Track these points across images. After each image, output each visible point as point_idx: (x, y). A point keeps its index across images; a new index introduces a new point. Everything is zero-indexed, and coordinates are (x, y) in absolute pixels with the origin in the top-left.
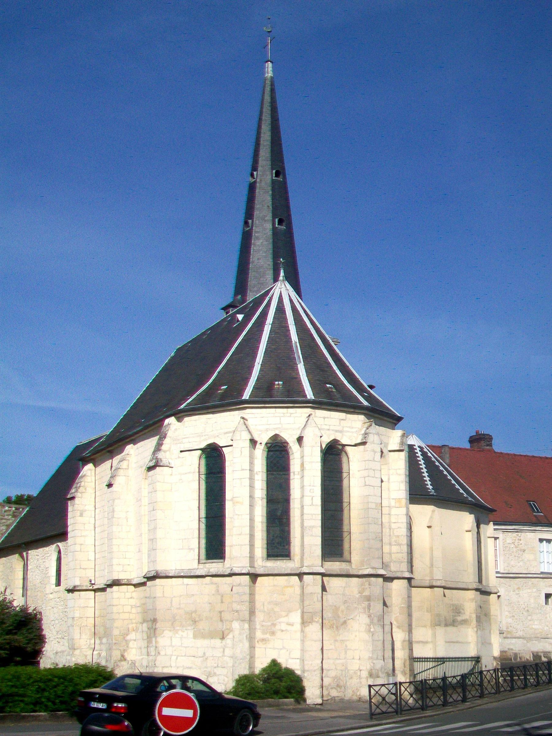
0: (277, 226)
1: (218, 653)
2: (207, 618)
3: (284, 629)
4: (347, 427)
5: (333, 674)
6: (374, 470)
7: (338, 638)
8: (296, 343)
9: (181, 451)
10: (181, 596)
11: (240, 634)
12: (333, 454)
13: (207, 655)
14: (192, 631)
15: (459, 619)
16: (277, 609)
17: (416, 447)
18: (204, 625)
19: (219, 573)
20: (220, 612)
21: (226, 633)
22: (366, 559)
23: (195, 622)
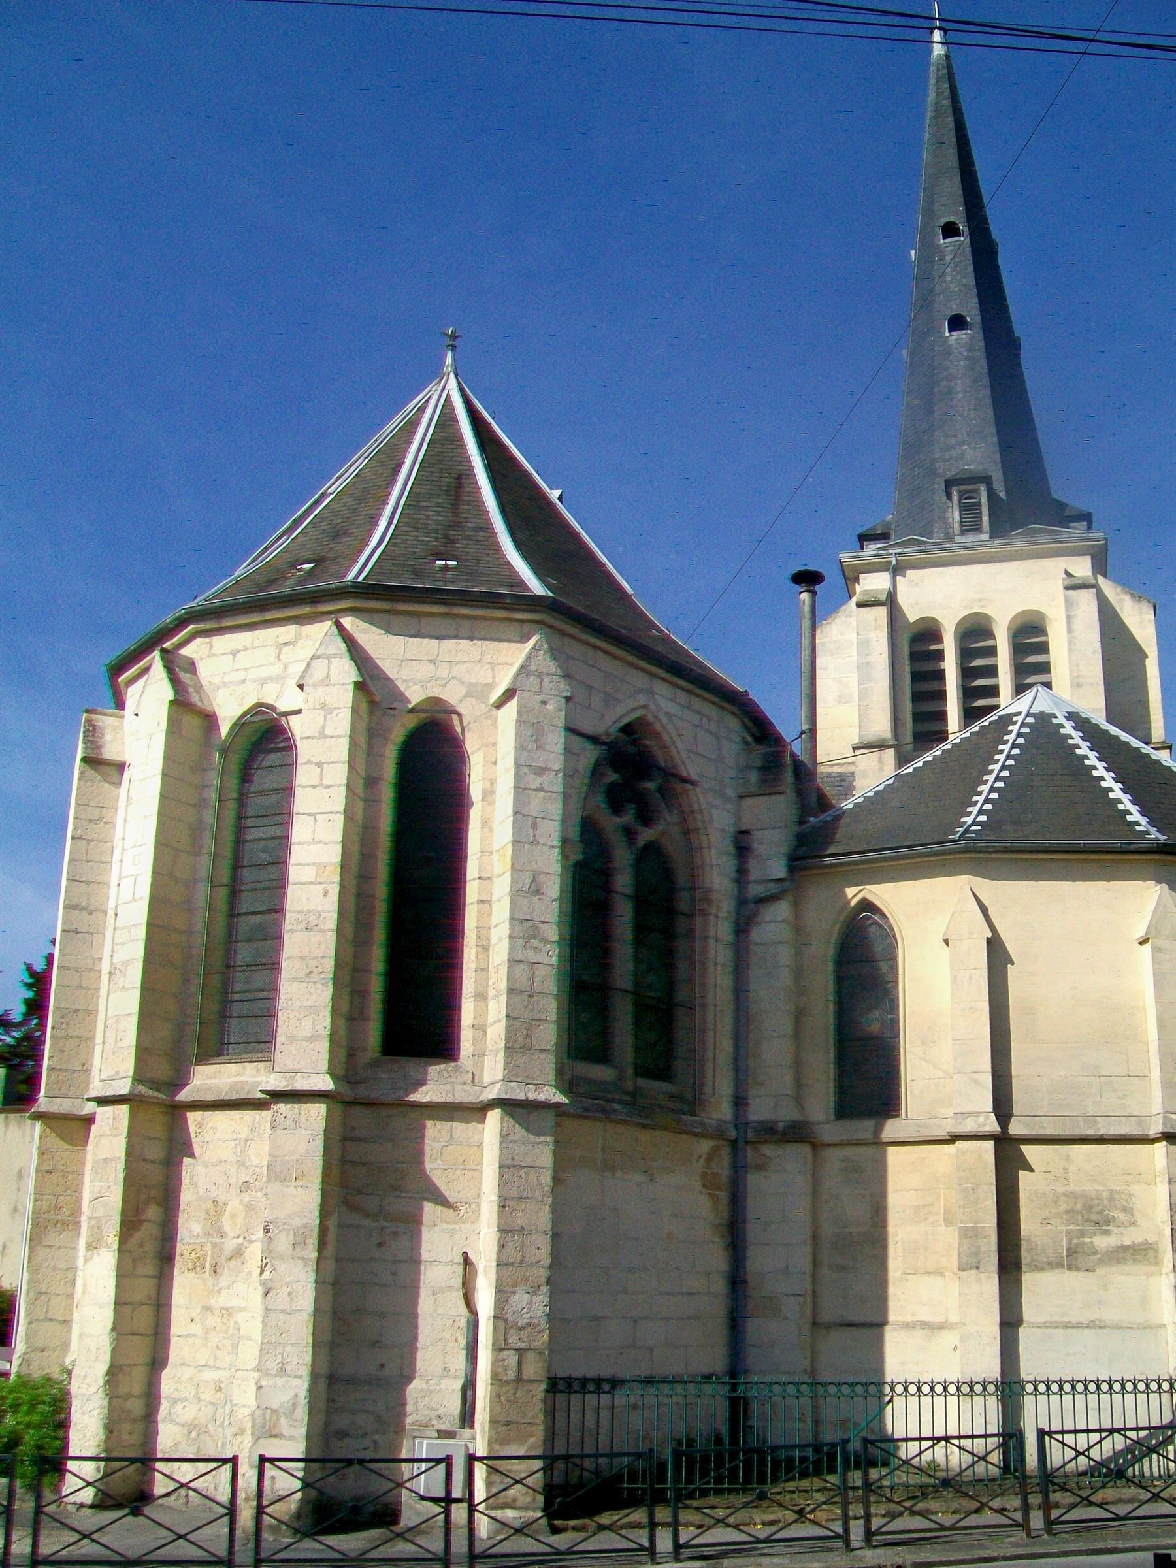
0: (947, 334)
5: (186, 1413)
6: (320, 765)
7: (213, 1302)
8: (324, 495)
15: (1102, 1242)
17: (1060, 719)
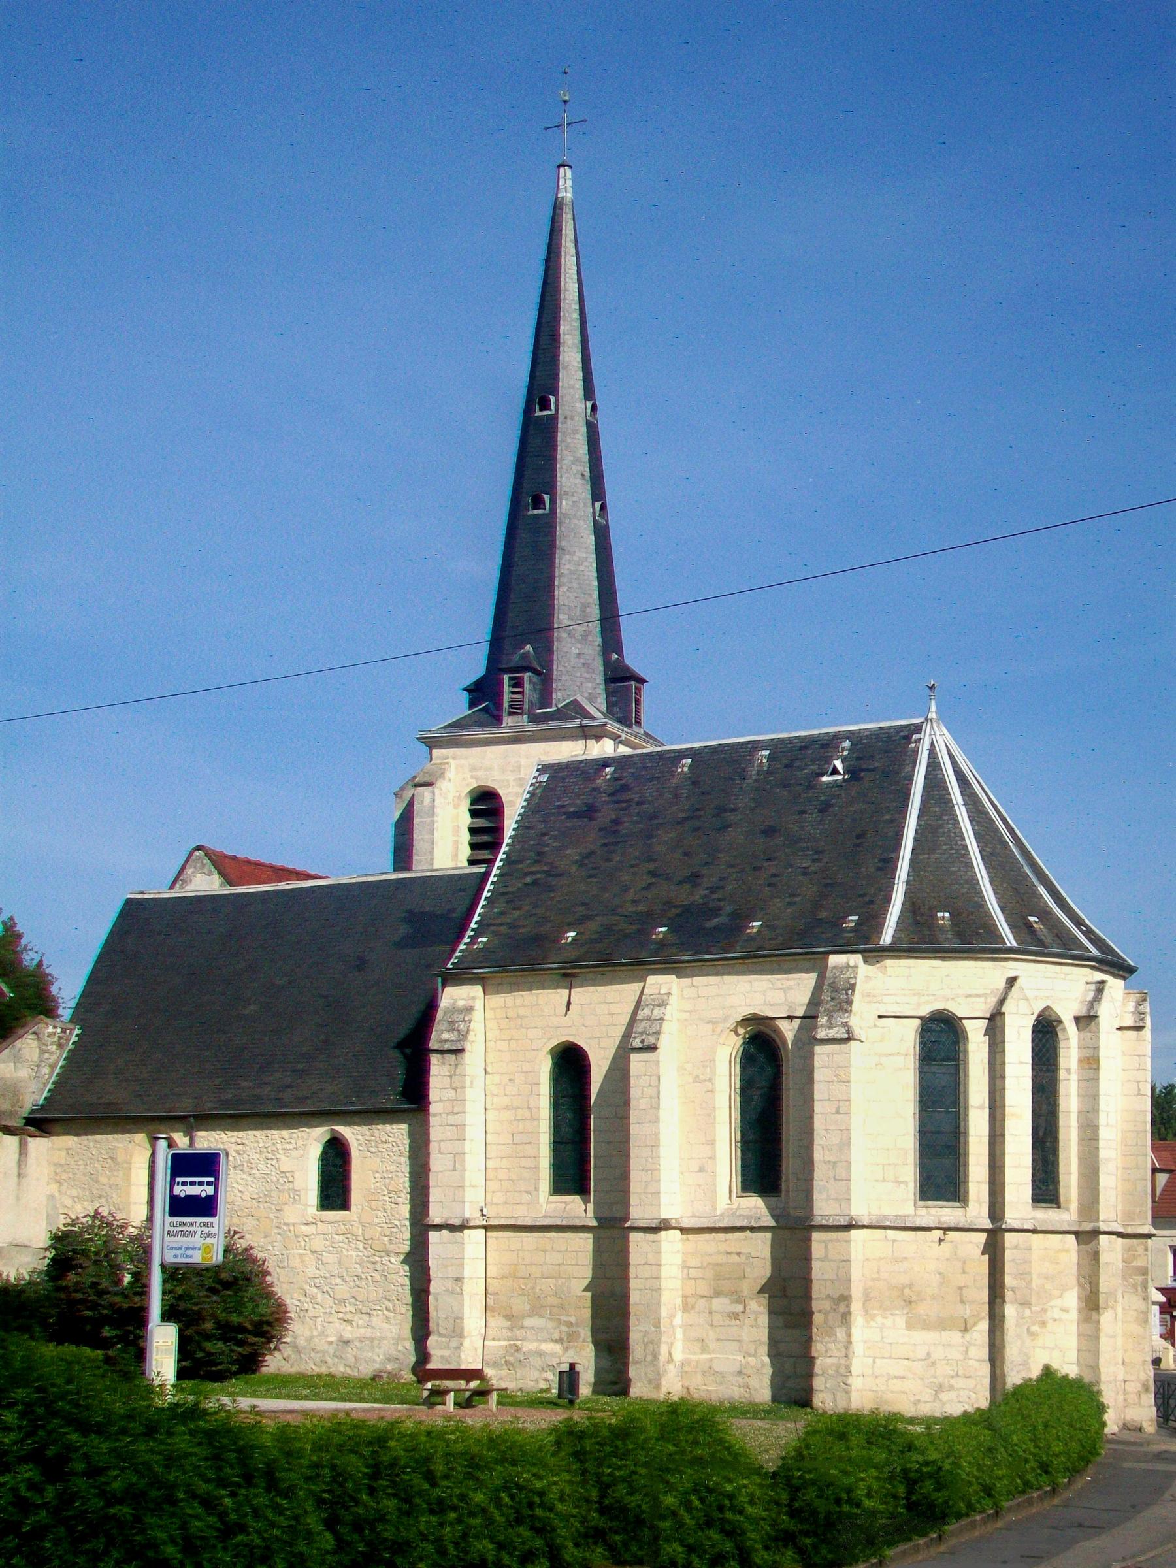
1: (955, 1354)
2: (933, 1298)
3: (1056, 1317)
4: (1058, 986)
9: (880, 1017)
10: (881, 1259)
11: (1017, 1325)
12: (1046, 1031)
13: (934, 1356)
14: (904, 1318)
16: (1048, 1287)
18: (922, 1309)
19: (961, 1225)
20: (960, 1288)
21: (970, 1322)
22: (1138, 1210)
23: (910, 1302)
